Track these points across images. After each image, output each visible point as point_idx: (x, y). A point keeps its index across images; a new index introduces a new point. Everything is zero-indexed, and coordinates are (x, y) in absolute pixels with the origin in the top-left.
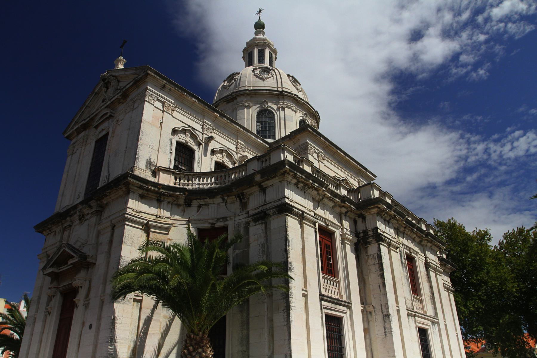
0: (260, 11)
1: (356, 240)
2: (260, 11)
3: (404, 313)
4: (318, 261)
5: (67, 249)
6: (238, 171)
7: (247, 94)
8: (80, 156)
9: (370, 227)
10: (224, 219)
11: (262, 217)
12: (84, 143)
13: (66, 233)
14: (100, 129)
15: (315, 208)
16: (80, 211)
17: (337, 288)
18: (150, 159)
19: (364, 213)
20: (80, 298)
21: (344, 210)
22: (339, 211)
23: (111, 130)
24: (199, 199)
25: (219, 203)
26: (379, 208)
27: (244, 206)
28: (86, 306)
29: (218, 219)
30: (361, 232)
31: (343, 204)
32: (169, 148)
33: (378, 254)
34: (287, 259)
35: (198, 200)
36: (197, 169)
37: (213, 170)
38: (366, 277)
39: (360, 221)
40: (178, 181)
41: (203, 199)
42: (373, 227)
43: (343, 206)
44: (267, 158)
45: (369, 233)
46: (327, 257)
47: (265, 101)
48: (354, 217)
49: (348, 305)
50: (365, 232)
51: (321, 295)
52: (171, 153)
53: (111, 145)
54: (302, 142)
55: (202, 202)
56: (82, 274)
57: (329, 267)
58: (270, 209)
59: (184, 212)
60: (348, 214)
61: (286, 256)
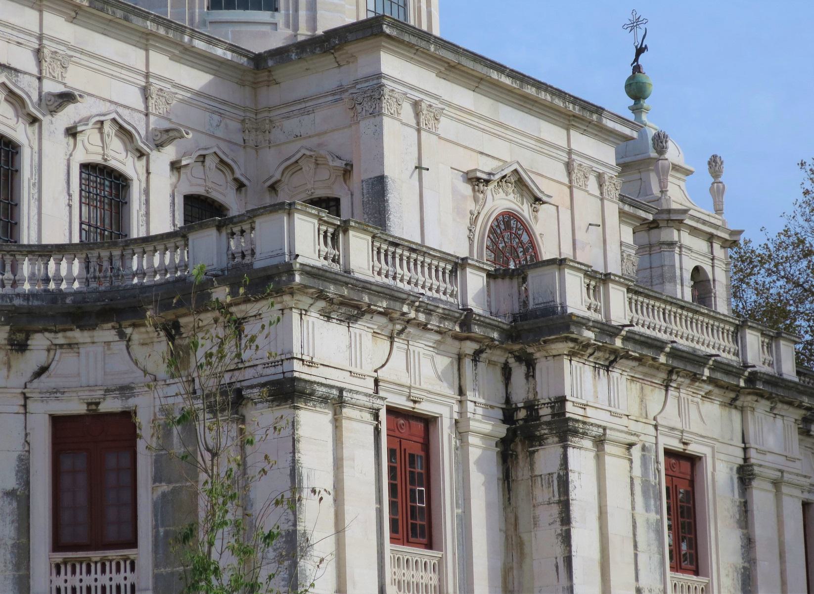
1: (502, 431)
4: (380, 512)
6: (161, 247)
9: (545, 393)
10: (125, 390)
11: (234, 401)
17: (435, 577)
19: (530, 350)
21: (470, 347)
22: (456, 351)
24: (50, 331)
25: (108, 343)
26: (575, 340)
27: (178, 359)
29: (107, 391)
30: (520, 405)
31: (465, 334)
33: (559, 476)
34: (295, 525)
35: (47, 334)
37: (76, 240)
38: (525, 537)
39: (519, 372)
41: (64, 330)
42: (553, 394)
43: (467, 338)
44: (246, 227)
45: (541, 412)
46: (413, 492)
48: (502, 360)
50: (531, 406)
54: (361, 68)
55: (60, 339)
58: (252, 387)
59: (9, 367)
60: (484, 355)
61: (291, 517)
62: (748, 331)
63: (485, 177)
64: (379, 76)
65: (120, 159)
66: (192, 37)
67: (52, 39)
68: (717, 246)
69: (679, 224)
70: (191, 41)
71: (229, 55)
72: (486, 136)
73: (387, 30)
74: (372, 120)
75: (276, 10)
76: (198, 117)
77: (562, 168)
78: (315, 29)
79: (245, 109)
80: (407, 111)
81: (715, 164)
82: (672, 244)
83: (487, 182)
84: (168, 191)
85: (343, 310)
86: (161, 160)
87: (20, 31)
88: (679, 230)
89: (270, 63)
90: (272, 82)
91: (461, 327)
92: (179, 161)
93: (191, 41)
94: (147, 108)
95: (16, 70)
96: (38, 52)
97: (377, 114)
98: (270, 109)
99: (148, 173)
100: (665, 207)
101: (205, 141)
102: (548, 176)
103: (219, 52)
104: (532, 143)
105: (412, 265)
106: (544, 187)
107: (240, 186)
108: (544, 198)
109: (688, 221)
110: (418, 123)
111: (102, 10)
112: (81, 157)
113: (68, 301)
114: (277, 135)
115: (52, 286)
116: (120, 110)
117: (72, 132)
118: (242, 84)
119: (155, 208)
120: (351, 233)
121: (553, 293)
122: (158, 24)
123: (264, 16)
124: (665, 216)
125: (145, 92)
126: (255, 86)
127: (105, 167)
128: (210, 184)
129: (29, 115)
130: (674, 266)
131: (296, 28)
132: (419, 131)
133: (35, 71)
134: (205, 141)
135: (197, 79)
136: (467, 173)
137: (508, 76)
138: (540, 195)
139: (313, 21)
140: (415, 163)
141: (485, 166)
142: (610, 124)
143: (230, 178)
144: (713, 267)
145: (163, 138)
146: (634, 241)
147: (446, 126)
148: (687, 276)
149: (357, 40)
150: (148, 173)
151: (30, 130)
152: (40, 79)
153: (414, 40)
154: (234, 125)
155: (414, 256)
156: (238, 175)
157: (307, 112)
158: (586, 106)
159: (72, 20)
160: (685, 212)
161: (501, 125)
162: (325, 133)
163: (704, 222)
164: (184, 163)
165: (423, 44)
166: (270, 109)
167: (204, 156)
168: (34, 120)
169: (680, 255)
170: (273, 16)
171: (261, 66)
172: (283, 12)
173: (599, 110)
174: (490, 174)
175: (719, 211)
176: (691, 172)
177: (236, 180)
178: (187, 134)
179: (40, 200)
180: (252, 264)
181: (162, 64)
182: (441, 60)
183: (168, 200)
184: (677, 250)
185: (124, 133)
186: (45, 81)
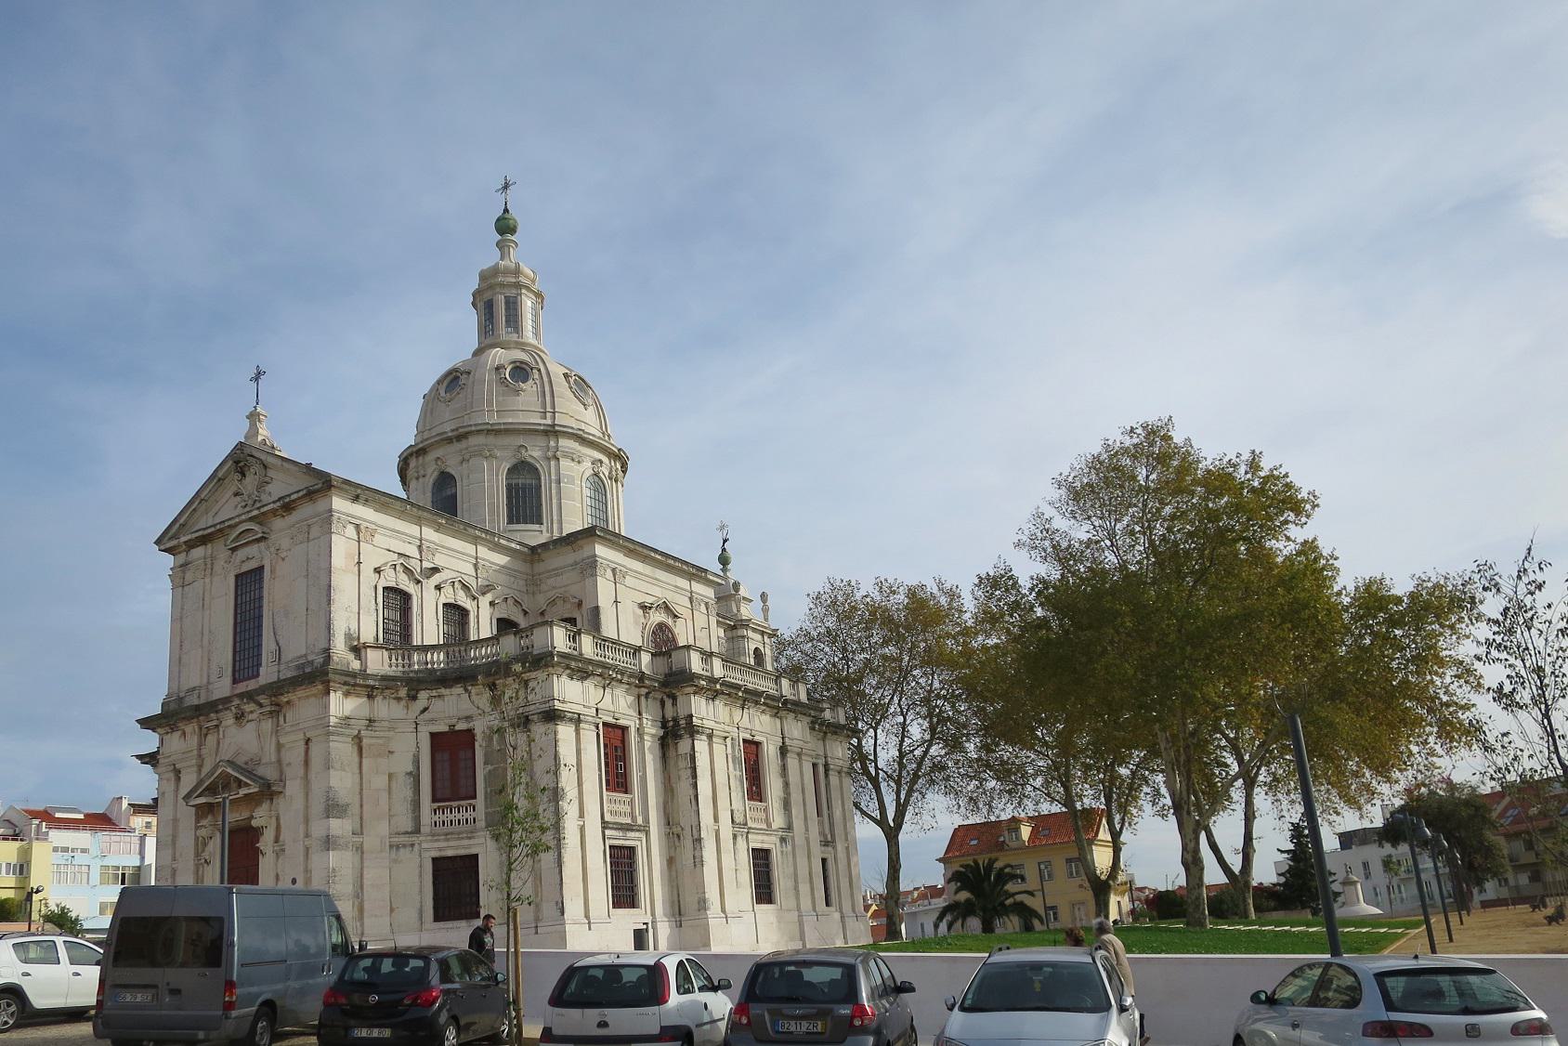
0: (506, 187)
1: (661, 733)
2: (506, 187)
3: (726, 829)
5: (229, 770)
9: (682, 713)
10: (468, 718)
11: (524, 722)
13: (211, 739)
14: (241, 554)
16: (238, 707)
20: (266, 843)
21: (644, 691)
28: (280, 853)
36: (416, 641)
39: (669, 703)
49: (645, 829)
50: (675, 720)
51: (603, 821)
53: (275, 594)
56: (265, 806)
57: (617, 779)
81: (764, 597)
86: (485, 601)
102: (680, 603)
106: (679, 610)
107: (525, 613)
112: (443, 600)
117: (438, 588)
123: (536, 527)
126: (532, 562)
135: (502, 559)
139: (561, 529)
141: (650, 600)
145: (485, 590)
147: (629, 581)
154: (522, 583)
168: (418, 582)
173: (706, 571)
185: (465, 587)
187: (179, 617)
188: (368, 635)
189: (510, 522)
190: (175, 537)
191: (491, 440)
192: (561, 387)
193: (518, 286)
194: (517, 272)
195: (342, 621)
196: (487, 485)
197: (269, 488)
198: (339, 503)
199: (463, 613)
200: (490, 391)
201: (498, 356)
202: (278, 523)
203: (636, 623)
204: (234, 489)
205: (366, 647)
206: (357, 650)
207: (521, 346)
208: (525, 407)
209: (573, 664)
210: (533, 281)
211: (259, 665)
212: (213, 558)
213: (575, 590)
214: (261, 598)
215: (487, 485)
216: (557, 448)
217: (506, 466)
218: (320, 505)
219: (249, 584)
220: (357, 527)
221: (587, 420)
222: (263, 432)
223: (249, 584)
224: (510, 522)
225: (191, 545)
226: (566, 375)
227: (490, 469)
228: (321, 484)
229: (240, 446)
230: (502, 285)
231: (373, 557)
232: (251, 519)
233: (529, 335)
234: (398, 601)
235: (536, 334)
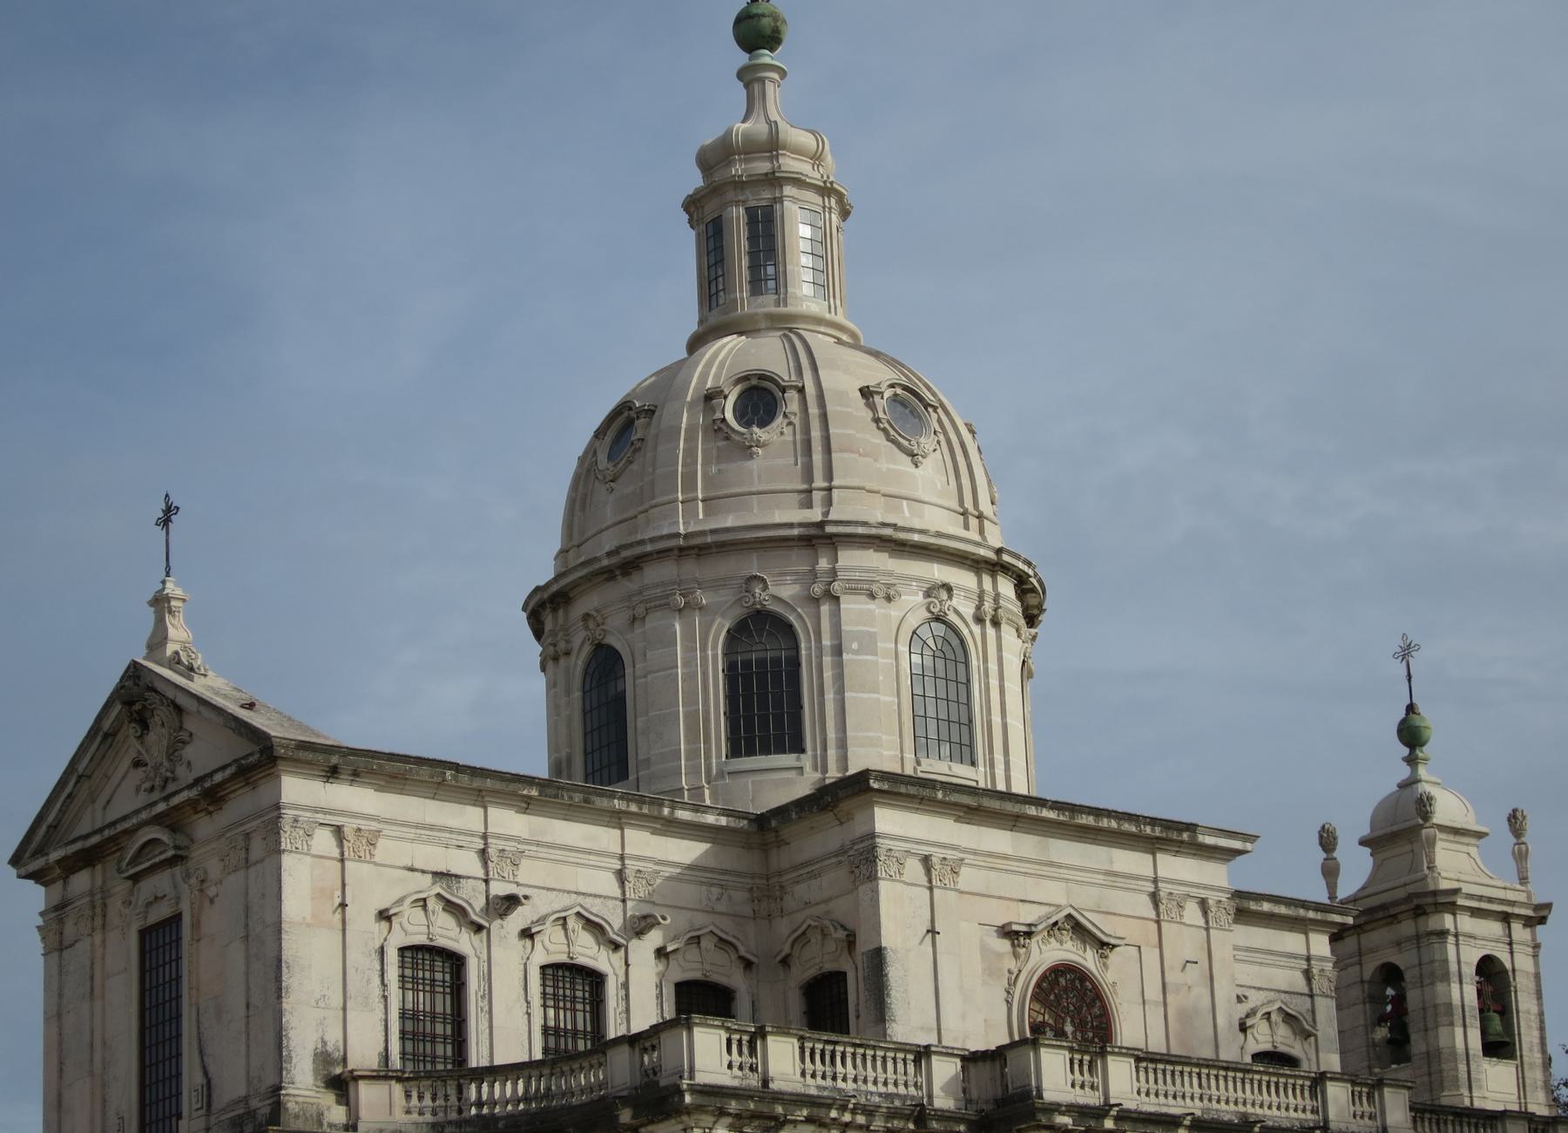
7: (681, 549)
8: (92, 967)
12: (98, 922)
14: (148, 887)
15: (1072, 818)
18: (324, 1043)
23: (185, 907)
32: (377, 981)
37: (538, 1055)
40: (415, 1101)
47: (763, 580)
52: (385, 998)
53: (209, 965)
62: (1329, 1084)
63: (1024, 929)
64: (872, 835)
65: (588, 952)
66: (673, 808)
67: (498, 837)
68: (1517, 927)
69: (1453, 908)
70: (672, 813)
71: (723, 821)
72: (1030, 880)
73: (875, 785)
74: (869, 885)
75: (803, 751)
76: (691, 893)
77: (1146, 900)
78: (846, 769)
79: (753, 876)
80: (914, 868)
81: (1515, 821)
82: (1443, 934)
83: (1029, 934)
84: (654, 980)
85: (756, 1123)
86: (643, 951)
87: (460, 833)
88: (1454, 914)
89: (774, 823)
90: (781, 843)
91: (915, 1123)
92: (664, 948)
93: (672, 813)
94: (624, 893)
95: (457, 876)
96: (483, 853)
97: (873, 878)
98: (780, 873)
99: (627, 965)
100: (1432, 888)
101: (700, 919)
102: (1120, 910)
103: (710, 819)
104: (1099, 878)
105: (859, 1061)
106: (1106, 927)
107: (748, 965)
108: (1113, 941)
109: (1460, 902)
110: (930, 881)
111: (556, 796)
112: (540, 958)
113: (500, 1125)
114: (789, 903)
115: (485, 1111)
116: (588, 902)
117: (527, 934)
118: (748, 847)
119: (638, 999)
120: (770, 1038)
121: (1029, 1076)
122: (629, 801)
123: (788, 759)
124: (1430, 900)
125: (621, 876)
126: (765, 848)
127: (574, 965)
128: (708, 967)
129: (473, 923)
130: (1446, 961)
131: (825, 770)
132: (931, 889)
133: (481, 873)
134: (700, 919)
135: (688, 851)
136: (1003, 927)
137: (1052, 808)
138: (1105, 939)
139: (843, 760)
140: (927, 925)
141: (1023, 916)
142: (1209, 840)
143: (734, 956)
144: (1512, 953)
145: (640, 926)
146: (1333, 951)
147: (969, 877)
148: (1469, 970)
149: (847, 797)
150: (627, 965)
151: (476, 939)
152: (486, 881)
153: (912, 790)
154: (740, 896)
155: (861, 1051)
156: (743, 952)
157: (813, 876)
158: (1168, 825)
159: (525, 811)
160: (1456, 891)
161: (1051, 864)
162: (830, 899)
163: (1490, 900)
164: (669, 949)
165: (926, 792)
166: (780, 873)
167: (698, 937)
168: (479, 928)
169: (1457, 945)
170: (798, 759)
171: (766, 829)
172: (809, 752)
173: (1191, 827)
174: (1030, 925)
175: (1523, 880)
176: (1486, 834)
177: (741, 958)
178: (664, 918)
179: (490, 1012)
180: (657, 1083)
181: (646, 845)
182: (956, 805)
183: (654, 992)
184: (1451, 939)
185: (595, 927)
186: (492, 883)
187: (56, 1015)
188: (364, 1051)
189: (735, 752)
190: (41, 851)
191: (690, 568)
192: (853, 424)
193: (774, 180)
194: (773, 146)
195: (308, 1026)
196: (688, 670)
197: (189, 752)
198: (296, 789)
199: (595, 980)
200: (690, 453)
201: (728, 356)
202: (204, 827)
203: (990, 971)
204: (132, 754)
205: (356, 1079)
206: (341, 1084)
207: (785, 324)
208: (767, 492)
209: (733, 1106)
210: (817, 158)
211: (179, 1116)
212: (105, 893)
213: (840, 908)
214: (178, 978)
215: (688, 670)
216: (833, 573)
217: (721, 628)
218: (263, 795)
219: (160, 945)
220: (338, 831)
221: (923, 494)
222: (178, 633)
223: (160, 945)
224: (735, 752)
225: (70, 866)
226: (866, 393)
227: (689, 637)
228: (260, 757)
229: (135, 672)
230: (739, 184)
231: (373, 886)
232: (157, 820)
233: (804, 292)
234: (437, 972)
235: (824, 286)
